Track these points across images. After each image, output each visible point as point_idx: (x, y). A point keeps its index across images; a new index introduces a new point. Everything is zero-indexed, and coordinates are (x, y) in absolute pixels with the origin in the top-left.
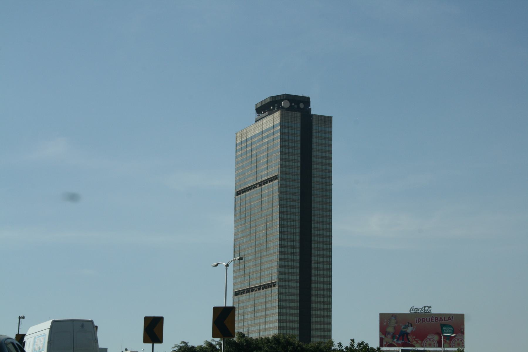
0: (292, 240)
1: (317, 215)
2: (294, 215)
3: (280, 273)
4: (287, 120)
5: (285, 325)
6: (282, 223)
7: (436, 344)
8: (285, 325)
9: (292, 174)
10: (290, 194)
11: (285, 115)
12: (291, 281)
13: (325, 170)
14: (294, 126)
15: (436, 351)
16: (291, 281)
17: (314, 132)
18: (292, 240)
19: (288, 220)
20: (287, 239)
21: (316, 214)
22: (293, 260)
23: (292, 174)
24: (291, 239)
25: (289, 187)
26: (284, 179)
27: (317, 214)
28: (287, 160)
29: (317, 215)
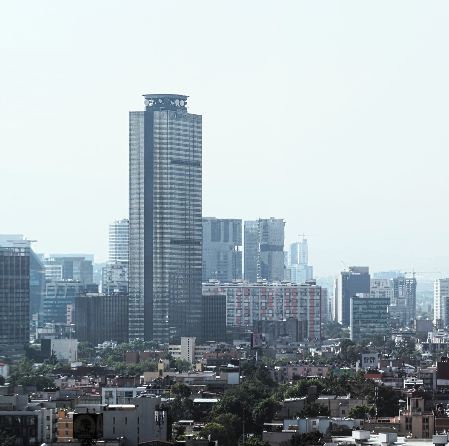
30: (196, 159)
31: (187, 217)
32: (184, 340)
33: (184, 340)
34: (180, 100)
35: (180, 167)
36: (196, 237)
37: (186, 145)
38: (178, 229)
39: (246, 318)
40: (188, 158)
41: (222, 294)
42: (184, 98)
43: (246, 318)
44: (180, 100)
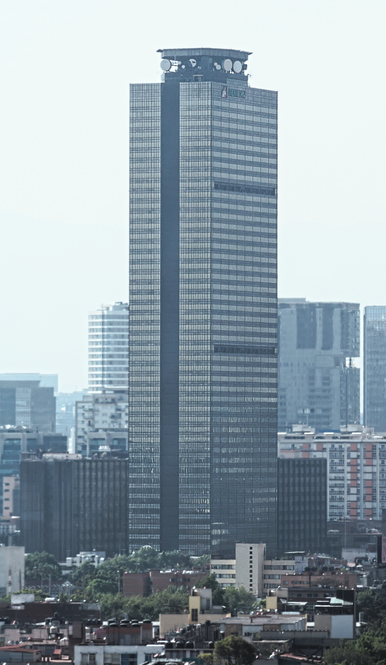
0: (148, 282)
1: (188, 239)
2: (151, 243)
3: (132, 293)
4: (139, 98)
5: (139, 399)
6: (132, 318)
7: (333, 495)
8: (139, 399)
9: (148, 182)
10: (145, 212)
11: (136, 90)
12: (147, 343)
13: (199, 137)
14: (150, 106)
15: (358, 381)
16: (147, 343)
17: (183, 109)
18: (148, 282)
19: (142, 211)
20: (141, 281)
21: (186, 238)
22: (151, 312)
23: (148, 181)
24: (147, 281)
25: (143, 202)
26: (136, 190)
27: (187, 237)
28: (141, 160)
29: (188, 239)
30: (265, 180)
31: (249, 299)
32: (242, 549)
33: (242, 549)
34: (233, 60)
35: (233, 196)
36: (266, 340)
37: (245, 163)
38: (230, 323)
39: (369, 505)
40: (249, 178)
41: (319, 455)
42: (242, 56)
43: (369, 505)
44: (233, 60)
